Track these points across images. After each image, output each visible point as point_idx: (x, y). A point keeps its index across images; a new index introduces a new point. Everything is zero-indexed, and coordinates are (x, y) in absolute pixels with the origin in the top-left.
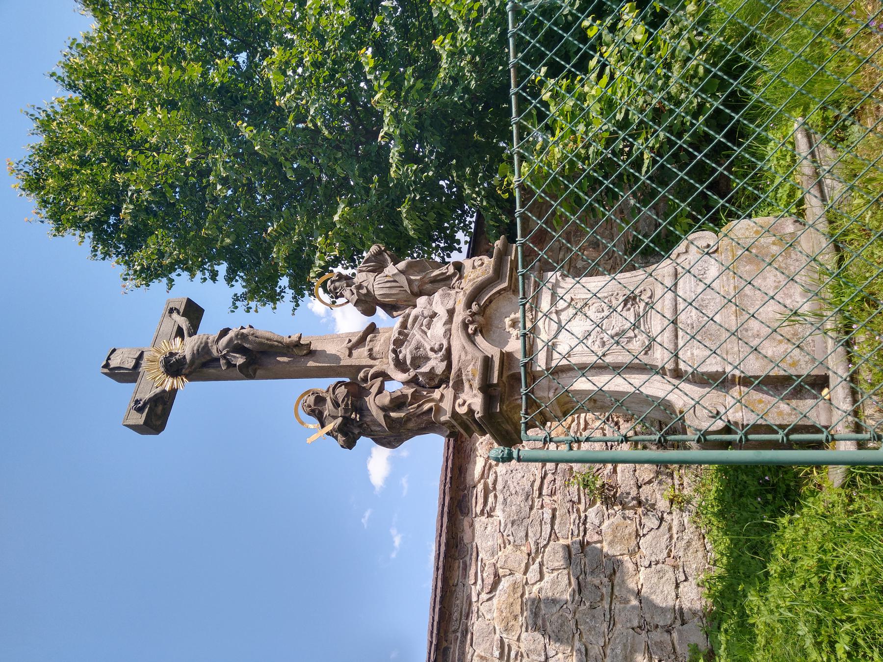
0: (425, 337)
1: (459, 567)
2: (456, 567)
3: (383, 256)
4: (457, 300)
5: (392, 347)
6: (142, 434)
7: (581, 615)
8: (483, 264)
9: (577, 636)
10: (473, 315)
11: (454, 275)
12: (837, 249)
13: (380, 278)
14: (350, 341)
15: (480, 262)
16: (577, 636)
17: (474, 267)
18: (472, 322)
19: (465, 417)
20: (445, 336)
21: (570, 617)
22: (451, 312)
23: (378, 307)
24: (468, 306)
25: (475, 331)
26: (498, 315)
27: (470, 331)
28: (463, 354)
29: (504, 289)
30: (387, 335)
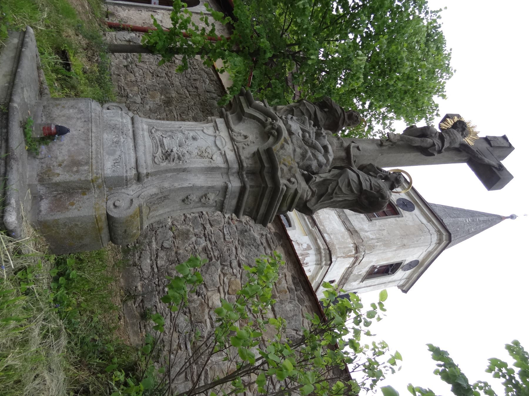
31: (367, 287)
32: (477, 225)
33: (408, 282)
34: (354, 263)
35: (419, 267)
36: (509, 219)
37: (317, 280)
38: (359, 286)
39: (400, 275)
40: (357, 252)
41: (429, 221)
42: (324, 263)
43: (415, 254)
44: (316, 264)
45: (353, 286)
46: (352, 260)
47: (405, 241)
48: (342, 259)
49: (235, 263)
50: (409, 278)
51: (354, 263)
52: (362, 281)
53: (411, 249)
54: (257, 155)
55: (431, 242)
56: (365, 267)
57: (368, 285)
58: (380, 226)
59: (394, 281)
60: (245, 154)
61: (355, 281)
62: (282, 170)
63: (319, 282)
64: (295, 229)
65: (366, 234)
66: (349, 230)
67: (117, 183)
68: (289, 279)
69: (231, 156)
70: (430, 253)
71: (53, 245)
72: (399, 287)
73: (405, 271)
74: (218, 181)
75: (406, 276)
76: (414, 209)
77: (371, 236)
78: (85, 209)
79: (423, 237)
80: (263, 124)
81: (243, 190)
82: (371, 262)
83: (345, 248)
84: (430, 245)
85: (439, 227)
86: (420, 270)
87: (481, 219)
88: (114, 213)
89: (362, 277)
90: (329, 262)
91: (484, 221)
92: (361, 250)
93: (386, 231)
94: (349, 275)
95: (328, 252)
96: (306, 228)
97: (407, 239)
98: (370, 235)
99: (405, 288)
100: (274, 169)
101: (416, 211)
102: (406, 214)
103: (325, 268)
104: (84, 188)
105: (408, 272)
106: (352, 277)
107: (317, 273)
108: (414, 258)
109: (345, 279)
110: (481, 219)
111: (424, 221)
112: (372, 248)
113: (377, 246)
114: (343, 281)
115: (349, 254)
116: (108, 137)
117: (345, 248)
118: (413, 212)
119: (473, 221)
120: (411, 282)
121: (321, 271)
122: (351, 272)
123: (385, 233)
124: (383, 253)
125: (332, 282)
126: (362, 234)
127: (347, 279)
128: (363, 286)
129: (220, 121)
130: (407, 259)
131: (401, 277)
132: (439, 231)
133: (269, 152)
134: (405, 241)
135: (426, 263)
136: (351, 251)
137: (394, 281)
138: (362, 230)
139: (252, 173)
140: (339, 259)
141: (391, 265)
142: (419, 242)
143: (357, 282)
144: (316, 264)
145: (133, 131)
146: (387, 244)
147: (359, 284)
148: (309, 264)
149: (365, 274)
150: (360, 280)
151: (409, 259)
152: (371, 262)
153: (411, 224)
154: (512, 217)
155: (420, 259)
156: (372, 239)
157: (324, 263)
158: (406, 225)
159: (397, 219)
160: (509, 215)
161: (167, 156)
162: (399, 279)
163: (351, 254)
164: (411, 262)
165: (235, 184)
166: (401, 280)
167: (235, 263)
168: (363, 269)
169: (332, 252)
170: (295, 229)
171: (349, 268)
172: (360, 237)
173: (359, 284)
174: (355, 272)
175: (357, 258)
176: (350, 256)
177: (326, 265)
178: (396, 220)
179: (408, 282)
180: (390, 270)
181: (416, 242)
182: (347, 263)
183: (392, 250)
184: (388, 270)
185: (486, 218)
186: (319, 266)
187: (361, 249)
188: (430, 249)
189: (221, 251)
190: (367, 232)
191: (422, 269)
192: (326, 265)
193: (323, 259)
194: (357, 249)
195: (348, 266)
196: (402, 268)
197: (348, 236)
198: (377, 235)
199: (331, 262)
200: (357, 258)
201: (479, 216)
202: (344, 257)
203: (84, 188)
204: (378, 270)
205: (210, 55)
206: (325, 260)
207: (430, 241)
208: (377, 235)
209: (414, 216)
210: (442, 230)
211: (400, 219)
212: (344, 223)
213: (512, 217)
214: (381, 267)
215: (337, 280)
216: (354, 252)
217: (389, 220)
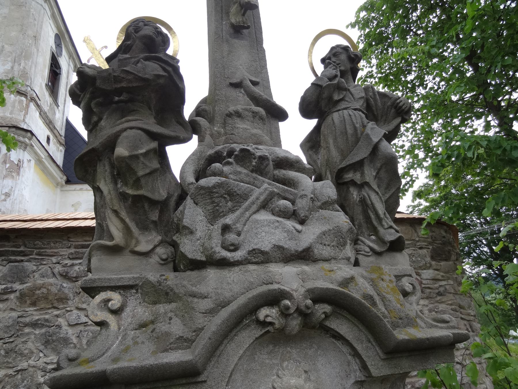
0: (254, 207)
1: (86, 241)
2: (85, 239)
3: (394, 118)
4: (333, 265)
5: (237, 147)
6: (262, 40)
7: (31, 373)
8: (405, 294)
9: (11, 372)
10: (304, 314)
11: (381, 240)
12: (383, 301)
13: (359, 117)
14: (255, 83)
15: (408, 288)
16: (11, 372)
17: (399, 277)
18: (285, 313)
19: (330, 178)
20: (253, 252)
21: (31, 362)
22: (305, 256)
23: (313, 123)
24: (319, 297)
25: (264, 324)
26: (310, 352)
27: (264, 313)
28: (205, 305)
29: (364, 367)
30: (266, 138)
31: (65, 104)
33: (73, 59)
37: (43, 157)
38: (61, 112)
40: (25, 96)
42: (27, 140)
43: (49, 33)
44: (24, 151)
45: (59, 119)
46: (32, 106)
47: (30, 33)
48: (28, 117)
50: (70, 56)
52: (58, 106)
53: (42, 33)
55: (42, 5)
56: (44, 95)
57: (63, 102)
59: (68, 72)
63: (47, 155)
70: (53, 16)
75: (67, 58)
79: (32, 10)
80: (275, 337)
82: (41, 84)
84: (44, 9)
86: (68, 39)
89: (54, 104)
90: (29, 134)
92: (23, 89)
93: (6, 46)
94: (47, 117)
95: (14, 129)
103: (34, 142)
106: (50, 115)
107: (36, 153)
109: (49, 124)
112: (25, 74)
113: (24, 68)
114: (51, 126)
115: (24, 105)
121: (35, 147)
124: (36, 66)
125: (48, 139)
128: (63, 107)
130: (51, 45)
131: (66, 62)
135: (63, 28)
136: (21, 102)
137: (68, 72)
140: (26, 120)
142: (37, 19)
143: (57, 112)
144: (24, 151)
145: (233, 370)
146: (25, 55)
147: (59, 111)
148: (21, 158)
150: (56, 107)
151: (52, 42)
152: (41, 84)
156: (12, 68)
162: (67, 66)
163: (25, 102)
164: (55, 43)
166: (69, 65)
168: (46, 98)
169: (15, 124)
171: (40, 114)
173: (59, 111)
174: (46, 108)
175: (32, 99)
176: (28, 106)
177: (30, 139)
179: (73, 59)
180: (56, 70)
181: (36, 22)
183: (36, 54)
186: (28, 148)
188: (49, 14)
191: (66, 36)
192: (30, 139)
193: (21, 139)
195: (38, 114)
199: (31, 132)
200: (32, 99)
202: (26, 113)
204: (51, 82)
205: (162, 251)
206: (24, 137)
207: (39, 6)
208: (9, 59)
215: (48, 132)
216: (23, 99)
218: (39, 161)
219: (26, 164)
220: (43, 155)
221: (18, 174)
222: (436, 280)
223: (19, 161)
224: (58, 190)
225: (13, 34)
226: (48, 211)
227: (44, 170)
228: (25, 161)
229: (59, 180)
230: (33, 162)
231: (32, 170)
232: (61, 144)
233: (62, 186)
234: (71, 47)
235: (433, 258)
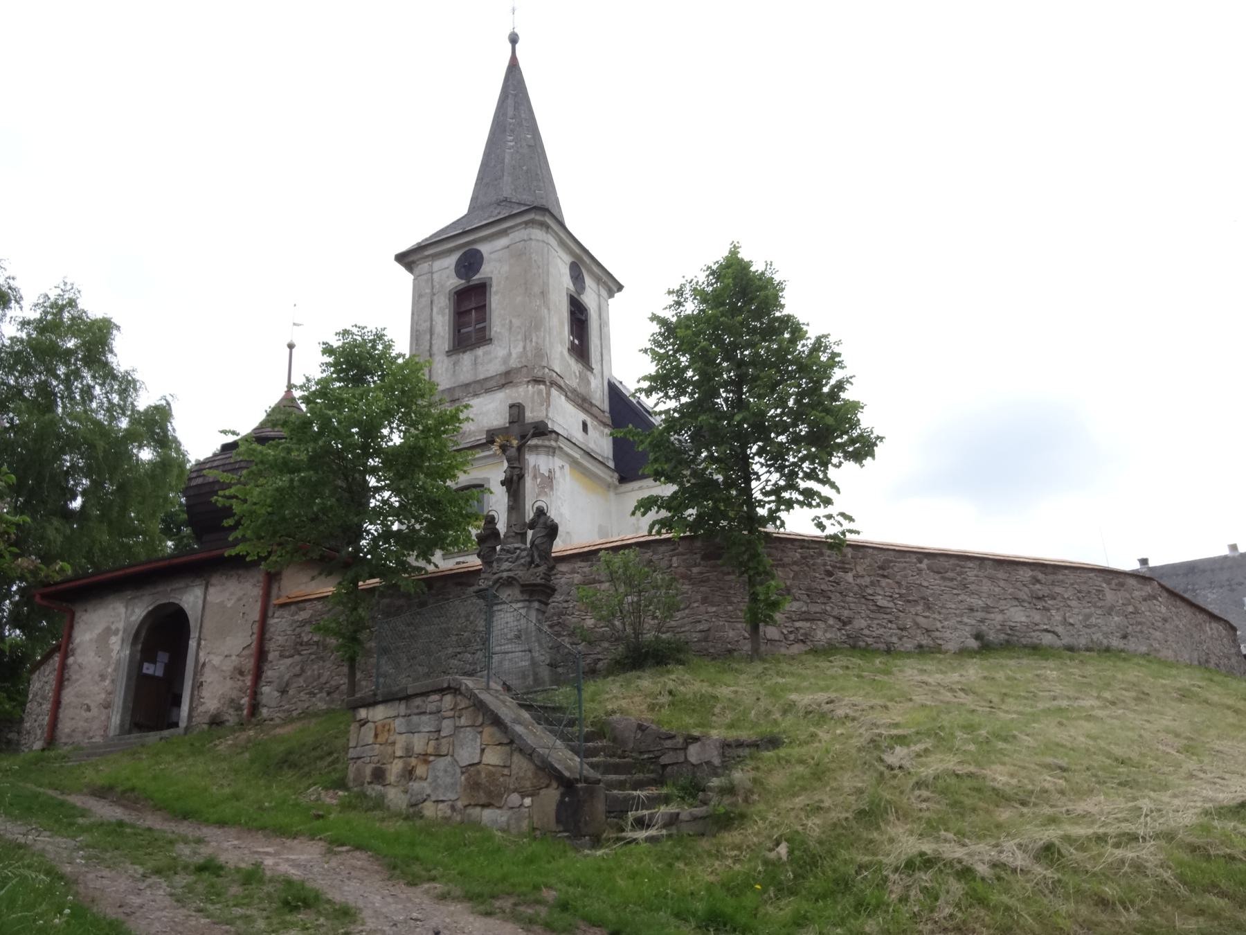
32: (520, 125)
33: (605, 283)
34: (560, 387)
35: (583, 264)
36: (517, 46)
38: (599, 376)
39: (590, 299)
40: (543, 382)
41: (505, 232)
42: (553, 443)
43: (561, 280)
47: (536, 290)
48: (551, 409)
49: (565, 605)
50: (598, 280)
51: (560, 387)
52: (591, 370)
54: (522, 592)
58: (503, 325)
60: (520, 597)
61: (589, 383)
62: (532, 580)
64: (488, 480)
65: (514, 356)
66: (503, 386)
67: (534, 663)
68: (583, 564)
69: (520, 605)
70: (562, 243)
71: (731, 391)
72: (611, 295)
73: (584, 288)
74: (533, 614)
76: (479, 252)
77: (520, 349)
78: (545, 673)
80: (502, 584)
81: (540, 601)
83: (533, 402)
85: (519, 220)
87: (510, 112)
88: (548, 662)
91: (516, 108)
92: (540, 374)
96: (490, 461)
97: (531, 283)
98: (517, 350)
99: (612, 286)
100: (535, 585)
101: (484, 248)
102: (486, 271)
103: (562, 444)
104: (535, 674)
105: (589, 282)
106: (581, 390)
107: (568, 455)
108: (565, 271)
109: (582, 402)
110: (510, 112)
111: (504, 241)
112: (540, 353)
114: (586, 405)
116: (506, 664)
117: (533, 402)
118: (485, 255)
119: (512, 131)
120: (605, 278)
121: (566, 449)
122: (574, 391)
123: (516, 322)
125: (585, 426)
126: (513, 363)
127: (584, 399)
129: (495, 608)
132: (526, 223)
133: (523, 586)
134: (536, 290)
135: (578, 251)
136: (540, 392)
138: (506, 360)
139: (531, 596)
141: (572, 313)
146: (535, 324)
149: (580, 365)
151: (567, 282)
153: (506, 268)
154: (514, 40)
155: (568, 259)
156: (524, 348)
157: (553, 443)
158: (507, 278)
159: (494, 289)
160: (510, 46)
161: (518, 637)
162: (596, 297)
165: (536, 605)
166: (599, 295)
167: (565, 605)
170: (488, 480)
171: (566, 396)
172: (518, 370)
174: (573, 382)
175: (553, 383)
176: (548, 394)
177: (556, 441)
178: (496, 293)
179: (605, 283)
182: (558, 399)
184: (579, 318)
185: (510, 101)
187: (538, 373)
188: (553, 242)
189: (554, 614)
190: (510, 354)
191: (585, 258)
192: (556, 441)
193: (547, 443)
194: (537, 381)
195: (563, 398)
196: (579, 294)
197: (514, 390)
198: (519, 337)
200: (553, 383)
201: (505, 114)
202: (549, 405)
203: (535, 674)
209: (493, 256)
210: (526, 218)
211: (494, 283)
212: (488, 391)
213: (514, 40)
214: (572, 332)
215: (582, 416)
216: (542, 387)
217: (493, 305)
218: (575, 463)
219: (558, 474)
220: (577, 455)
221: (552, 488)
222: (701, 573)
223: (550, 471)
224: (612, 494)
225: (519, 299)
226: (602, 531)
227: (585, 472)
228: (557, 469)
229: (609, 480)
230: (567, 467)
231: (568, 478)
232: (605, 425)
233: (616, 487)
234: (595, 269)
235: (703, 559)
